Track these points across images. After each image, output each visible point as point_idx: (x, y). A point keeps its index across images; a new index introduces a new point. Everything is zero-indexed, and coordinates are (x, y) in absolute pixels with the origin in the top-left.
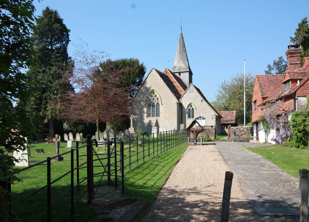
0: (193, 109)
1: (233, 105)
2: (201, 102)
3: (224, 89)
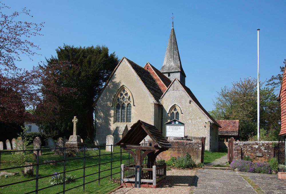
0: (177, 112)
1: (234, 114)
2: (189, 104)
3: (224, 96)
